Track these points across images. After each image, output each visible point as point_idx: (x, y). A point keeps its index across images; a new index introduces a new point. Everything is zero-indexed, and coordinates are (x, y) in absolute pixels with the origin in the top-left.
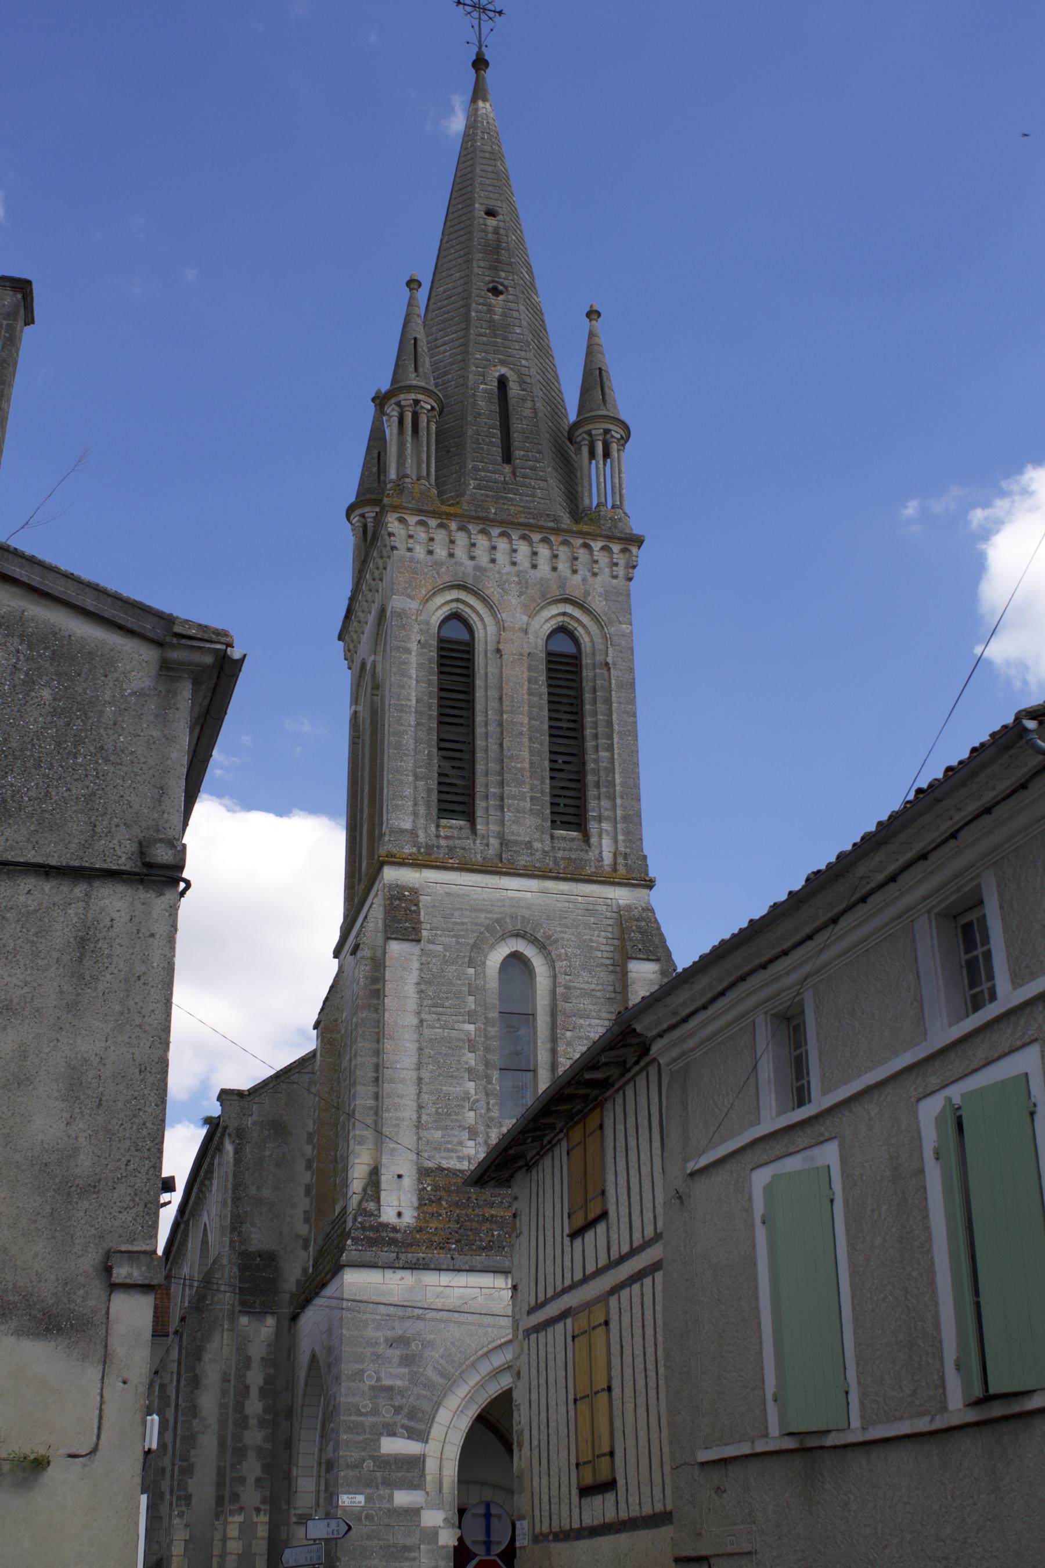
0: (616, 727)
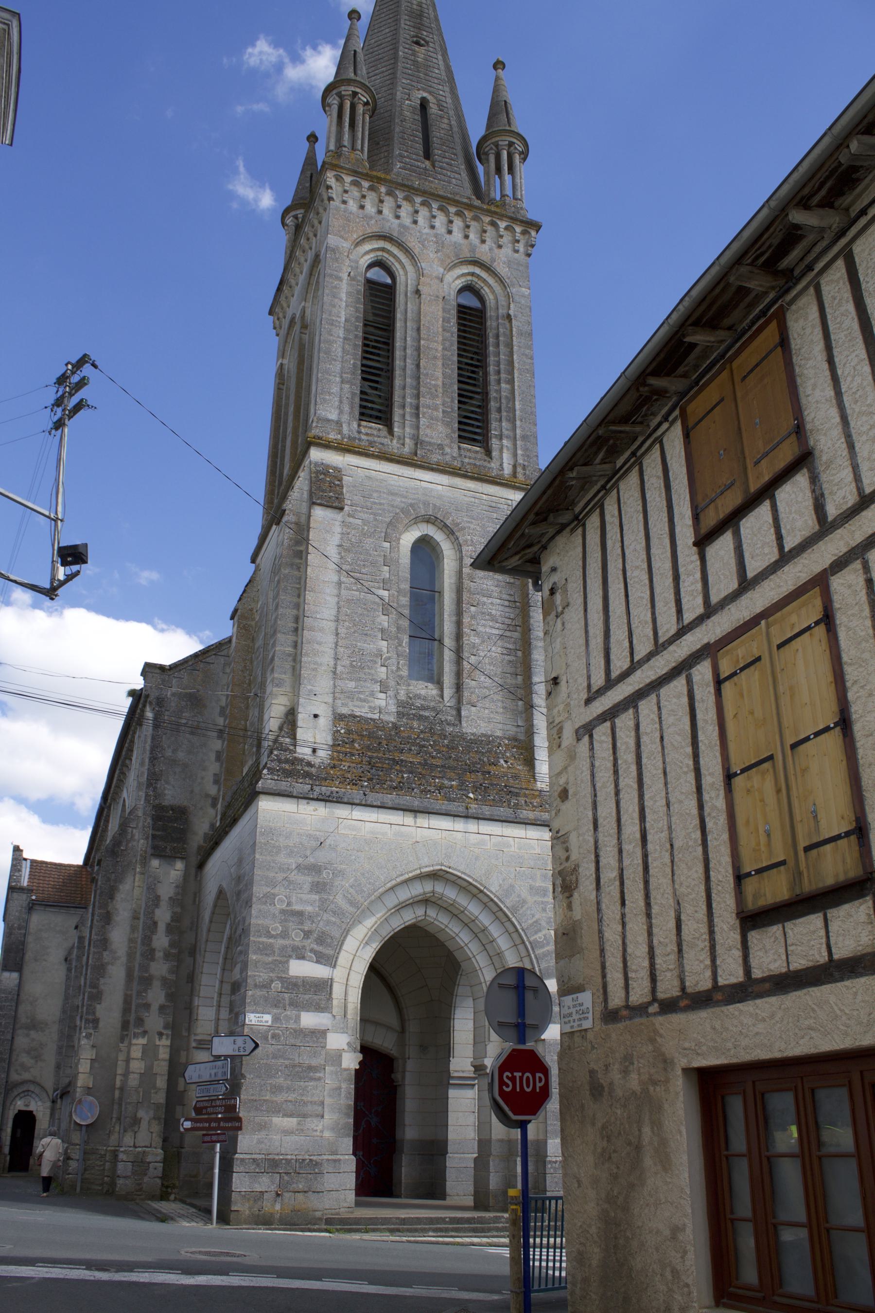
0: (516, 365)
